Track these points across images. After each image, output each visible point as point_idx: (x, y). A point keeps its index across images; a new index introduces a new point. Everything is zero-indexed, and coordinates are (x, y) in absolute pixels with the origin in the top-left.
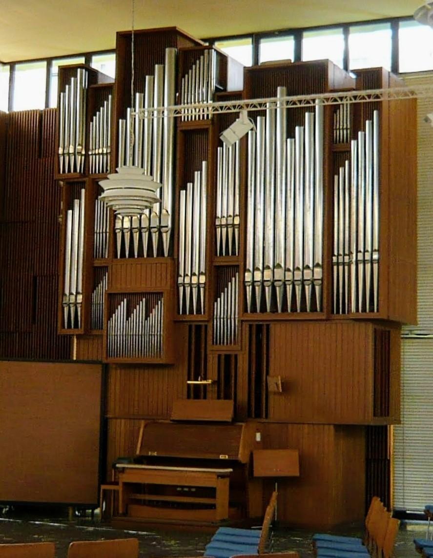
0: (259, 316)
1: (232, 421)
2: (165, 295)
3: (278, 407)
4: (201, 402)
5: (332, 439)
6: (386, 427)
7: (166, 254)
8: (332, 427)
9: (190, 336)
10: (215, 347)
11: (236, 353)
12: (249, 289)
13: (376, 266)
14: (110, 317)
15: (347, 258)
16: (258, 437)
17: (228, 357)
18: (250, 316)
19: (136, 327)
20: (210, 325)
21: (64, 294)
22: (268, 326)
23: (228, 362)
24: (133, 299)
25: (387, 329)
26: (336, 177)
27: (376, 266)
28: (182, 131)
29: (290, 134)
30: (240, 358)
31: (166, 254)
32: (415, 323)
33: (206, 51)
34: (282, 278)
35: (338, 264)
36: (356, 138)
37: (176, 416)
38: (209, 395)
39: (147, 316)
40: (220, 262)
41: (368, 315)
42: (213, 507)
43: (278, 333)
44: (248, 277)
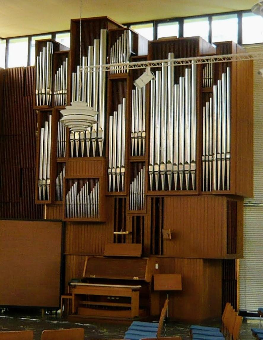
0: (157, 193)
1: (141, 256)
2: (100, 180)
3: (169, 248)
5: (202, 267)
6: (235, 260)
7: (101, 155)
8: (202, 260)
9: (116, 205)
10: (131, 212)
11: (143, 215)
12: (151, 176)
13: (228, 162)
14: (67, 193)
15: (211, 157)
16: (157, 266)
17: (138, 218)
18: (152, 193)
19: (83, 199)
20: (128, 198)
21: (39, 179)
22: (163, 198)
23: (138, 221)
24: (81, 182)
25: (235, 200)
26: (204, 108)
27: (228, 162)
28: (110, 80)
29: (176, 82)
30: (146, 218)
31: (101, 155)
33: (125, 31)
34: (171, 169)
35: (205, 161)
36: (216, 84)
37: (107, 254)
38: (127, 241)
39: (89, 192)
40: (133, 159)
41: (224, 192)
42: (129, 309)
43: (169, 203)
44: (151, 169)
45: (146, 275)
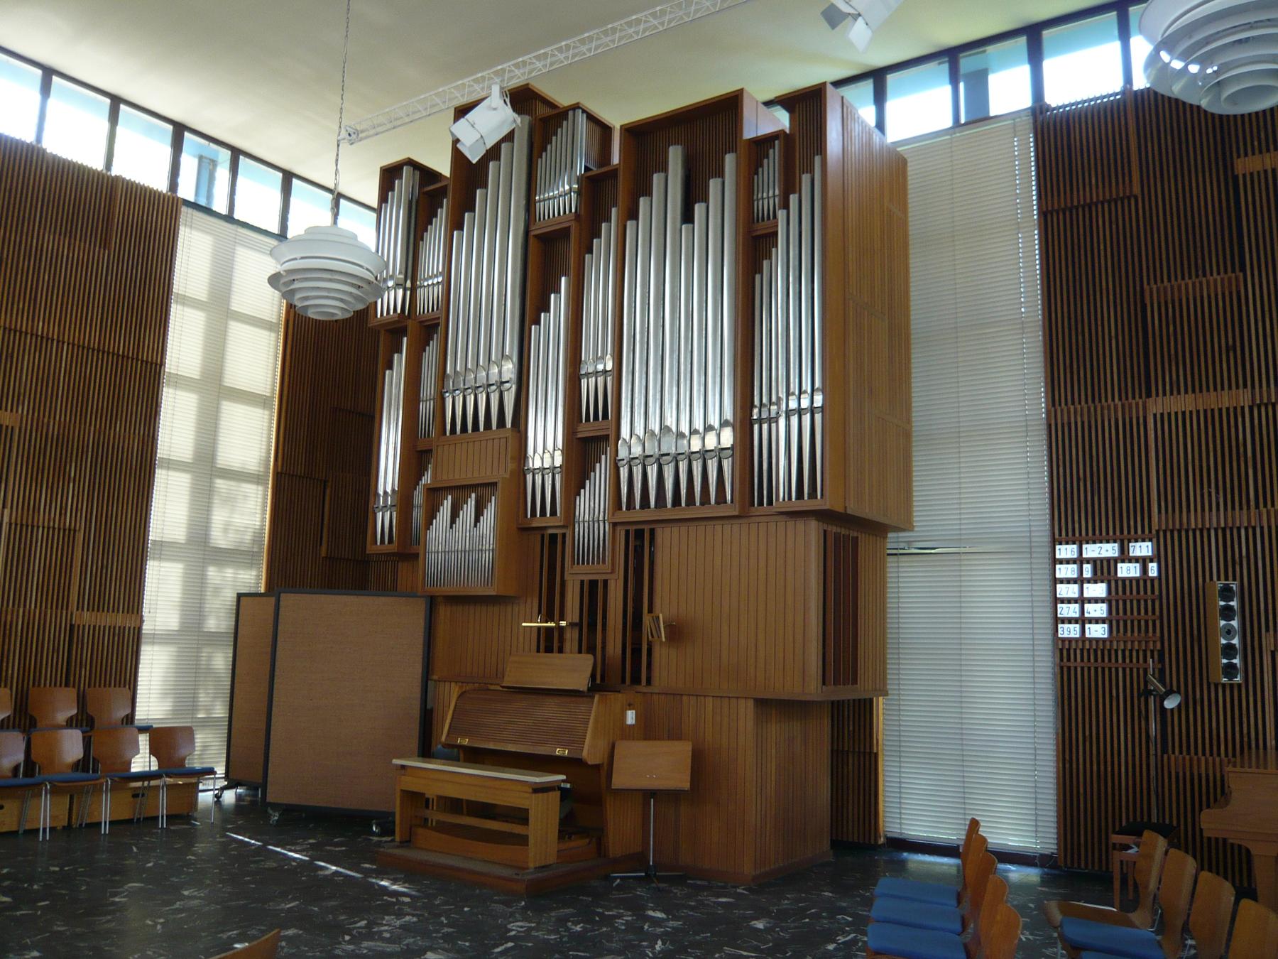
0: (638, 515)
1: (589, 689)
2: (500, 485)
3: (667, 665)
4: (555, 658)
5: (750, 724)
6: (871, 700)
7: (509, 425)
8: (751, 703)
9: (538, 547)
10: (576, 569)
11: (605, 577)
12: (624, 473)
13: (818, 417)
14: (429, 523)
15: (774, 408)
16: (631, 718)
17: (593, 584)
18: (625, 515)
19: (463, 539)
20: (568, 532)
21: (377, 494)
22: (652, 532)
23: (593, 591)
24: (459, 492)
25: (853, 534)
26: (758, 277)
27: (818, 417)
28: (536, 236)
29: (688, 217)
30: (611, 585)
31: (509, 425)
32: (907, 526)
33: (571, 113)
34: (673, 451)
35: (760, 421)
36: (786, 206)
37: (508, 682)
38: (567, 646)
39: (477, 520)
40: (585, 431)
41: (807, 504)
42: (523, 840)
43: (668, 543)
44: (623, 453)
45: (586, 747)
